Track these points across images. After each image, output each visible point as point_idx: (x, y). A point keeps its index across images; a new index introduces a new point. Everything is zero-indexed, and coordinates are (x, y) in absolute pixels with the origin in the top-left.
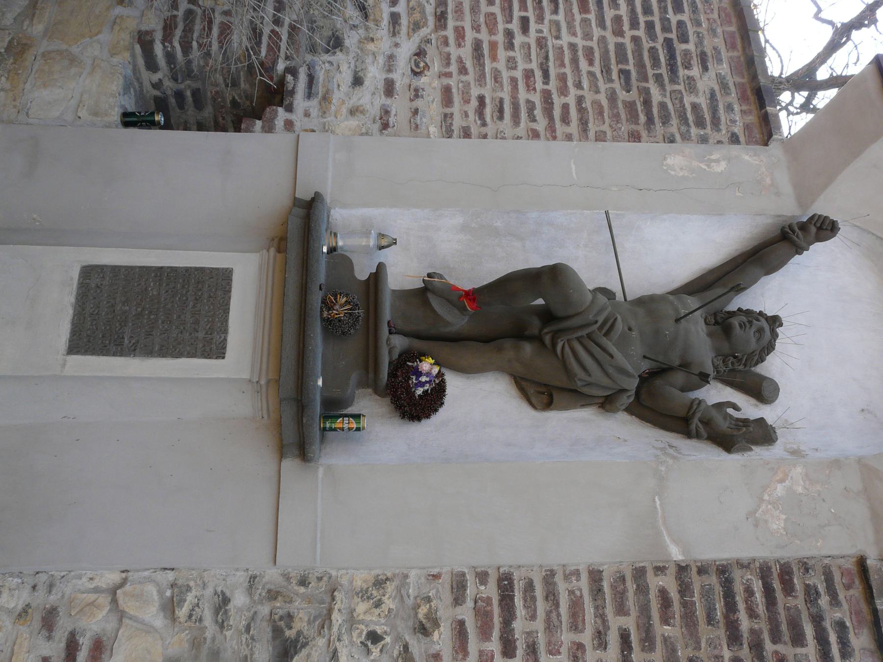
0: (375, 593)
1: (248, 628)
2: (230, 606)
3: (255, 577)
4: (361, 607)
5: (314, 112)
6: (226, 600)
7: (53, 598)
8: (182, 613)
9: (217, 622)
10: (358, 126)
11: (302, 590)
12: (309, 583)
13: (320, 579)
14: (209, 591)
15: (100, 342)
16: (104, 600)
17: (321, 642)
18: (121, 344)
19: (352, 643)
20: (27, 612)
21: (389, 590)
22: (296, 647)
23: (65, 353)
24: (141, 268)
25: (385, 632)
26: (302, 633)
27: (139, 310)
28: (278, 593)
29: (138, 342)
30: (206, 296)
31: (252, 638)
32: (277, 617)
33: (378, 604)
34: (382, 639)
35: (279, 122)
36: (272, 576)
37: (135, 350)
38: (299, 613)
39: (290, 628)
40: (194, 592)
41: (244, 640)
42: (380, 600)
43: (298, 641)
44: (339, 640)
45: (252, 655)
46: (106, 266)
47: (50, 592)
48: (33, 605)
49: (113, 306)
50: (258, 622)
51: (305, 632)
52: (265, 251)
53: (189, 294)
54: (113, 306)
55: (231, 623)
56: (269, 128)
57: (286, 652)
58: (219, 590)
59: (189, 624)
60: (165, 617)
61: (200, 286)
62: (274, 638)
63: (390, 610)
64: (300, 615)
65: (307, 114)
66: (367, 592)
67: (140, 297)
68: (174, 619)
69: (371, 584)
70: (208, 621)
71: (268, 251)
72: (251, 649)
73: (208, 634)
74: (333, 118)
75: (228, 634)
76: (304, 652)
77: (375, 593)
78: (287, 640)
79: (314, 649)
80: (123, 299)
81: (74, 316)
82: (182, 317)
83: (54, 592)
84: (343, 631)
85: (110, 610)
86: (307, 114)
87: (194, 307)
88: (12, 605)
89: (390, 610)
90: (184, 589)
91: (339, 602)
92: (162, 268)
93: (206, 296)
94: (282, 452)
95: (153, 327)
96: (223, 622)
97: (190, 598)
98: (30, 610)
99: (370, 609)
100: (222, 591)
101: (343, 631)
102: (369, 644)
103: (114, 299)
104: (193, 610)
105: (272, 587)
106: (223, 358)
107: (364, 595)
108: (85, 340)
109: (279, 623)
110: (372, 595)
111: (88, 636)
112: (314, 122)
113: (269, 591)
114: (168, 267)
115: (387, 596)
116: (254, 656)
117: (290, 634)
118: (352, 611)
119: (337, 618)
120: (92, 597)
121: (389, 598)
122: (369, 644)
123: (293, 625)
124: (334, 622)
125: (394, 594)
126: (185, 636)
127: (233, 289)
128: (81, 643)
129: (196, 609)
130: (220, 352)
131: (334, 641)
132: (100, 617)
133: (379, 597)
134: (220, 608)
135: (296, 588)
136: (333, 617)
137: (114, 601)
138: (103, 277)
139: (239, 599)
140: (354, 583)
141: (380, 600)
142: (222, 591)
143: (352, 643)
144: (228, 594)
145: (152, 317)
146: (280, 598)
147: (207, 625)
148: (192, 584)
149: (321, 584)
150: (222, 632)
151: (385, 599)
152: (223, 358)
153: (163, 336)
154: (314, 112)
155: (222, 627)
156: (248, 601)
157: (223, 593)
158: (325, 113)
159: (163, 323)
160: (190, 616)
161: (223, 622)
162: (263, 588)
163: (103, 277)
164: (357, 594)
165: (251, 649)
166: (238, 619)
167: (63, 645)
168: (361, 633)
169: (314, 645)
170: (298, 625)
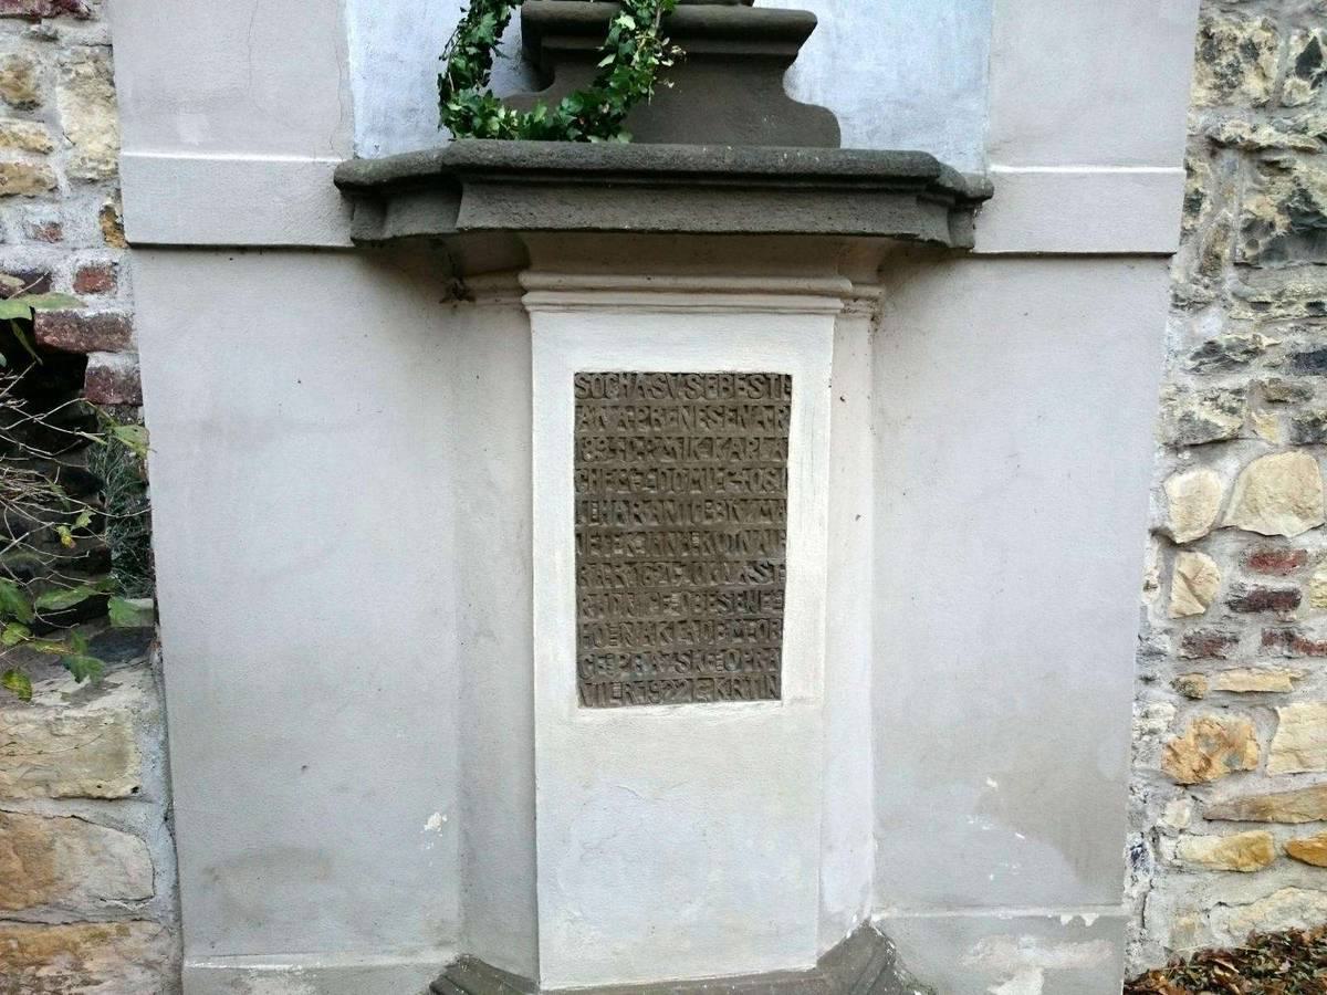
0: (1224, 61)
1: (1261, 306)
2: (1222, 340)
3: (1176, 297)
4: (1253, 85)
5: (44, 213)
6: (1212, 349)
7: (1168, 645)
8: (1224, 424)
9: (1246, 363)
10: (70, 86)
11: (1206, 206)
12: (1197, 191)
13: (1190, 170)
14: (1191, 382)
15: (752, 640)
16: (1184, 563)
17: (1301, 166)
18: (758, 596)
19: (1313, 105)
20: (1185, 684)
21: (1225, 28)
22: (1306, 214)
23: (777, 703)
24: (580, 579)
25: (1303, 37)
26: (1283, 202)
27: (679, 571)
28: (1208, 253)
29: (752, 563)
30: (645, 430)
31: (1279, 295)
32: (1250, 253)
33: (1251, 50)
34: (1314, 43)
35: (94, 306)
36: (1180, 271)
37: (771, 567)
38: (1248, 211)
39: (1272, 225)
40: (1195, 408)
41: (1282, 311)
42: (1243, 48)
43: (1296, 209)
44: (1304, 131)
45: (1308, 296)
46: (579, 655)
47: (1160, 653)
48: (1174, 676)
49: (671, 627)
50: (1247, 289)
51: (1282, 197)
52: (526, 299)
53: (640, 467)
54: (671, 627)
55: (1250, 337)
56: (115, 332)
57: (1319, 231)
58: (1191, 364)
59: (1244, 411)
60: (1223, 455)
61: (621, 445)
62: (1282, 256)
63: (1265, 27)
64: (1252, 208)
65: (53, 233)
66: (1223, 76)
67: (649, 573)
68: (1235, 438)
69: (1208, 69)
70: (1241, 379)
71: (524, 291)
72: (1298, 297)
73: (1265, 376)
74: (52, 160)
75: (1266, 341)
76: (1317, 197)
77: (1224, 61)
78: (1291, 231)
79: (1314, 179)
80: (653, 608)
81: (695, 700)
82: (696, 475)
83: (1160, 647)
84: (1289, 122)
85: (1204, 550)
86: (53, 233)
87: (671, 453)
88: (1171, 709)
89: (1265, 27)
90: (1187, 427)
91: (1239, 131)
92: (578, 536)
93: (645, 430)
94: (950, 254)
95: (721, 536)
96: (1247, 352)
97: (1203, 413)
98: (1183, 679)
99: (1258, 67)
100: (1192, 359)
101: (1289, 122)
102: (1319, 70)
103: (654, 626)
104: (1222, 407)
105: (1196, 264)
106: (788, 378)
107: (1227, 84)
108: (749, 669)
109: (1261, 248)
110: (1230, 65)
111: (1242, 580)
112: (83, 216)
113: (1202, 270)
114: (577, 521)
115: (1237, 33)
116: (1310, 290)
117: (1282, 223)
118: (1259, 106)
119: (1266, 135)
120: (1178, 583)
121: (1241, 29)
122: (1319, 70)
123: (1268, 219)
124: (1272, 141)
125: (1234, 18)
126: (1262, 416)
127: (629, 369)
128: (1254, 588)
129: (1220, 401)
130: (778, 386)
131: (1305, 141)
132: (1212, 564)
133: (1237, 51)
134: (1223, 358)
135: (1202, 219)
136: (1263, 143)
137: (1187, 547)
138: (605, 657)
139: (1212, 326)
140: (1203, 102)
141: (1243, 48)
142: (1192, 359)
143: (1313, 105)
144: (1199, 347)
145: (696, 540)
146: (1218, 249)
147: (1248, 380)
148: (1178, 413)
149: (1199, 171)
150: (1263, 352)
151: (1242, 37)
152: (788, 378)
153: (739, 513)
154: (44, 213)
155: (1255, 353)
156: (1214, 309)
157: (1198, 355)
158: (39, 182)
159: (709, 517)
160: (1233, 411)
161: (1247, 352)
162: (1196, 282)
163: (605, 657)
164: (1225, 95)
165: (1298, 297)
166: (1242, 325)
167: (1248, 618)
168: (1297, 87)
169: (1309, 179)
170: (1269, 212)
